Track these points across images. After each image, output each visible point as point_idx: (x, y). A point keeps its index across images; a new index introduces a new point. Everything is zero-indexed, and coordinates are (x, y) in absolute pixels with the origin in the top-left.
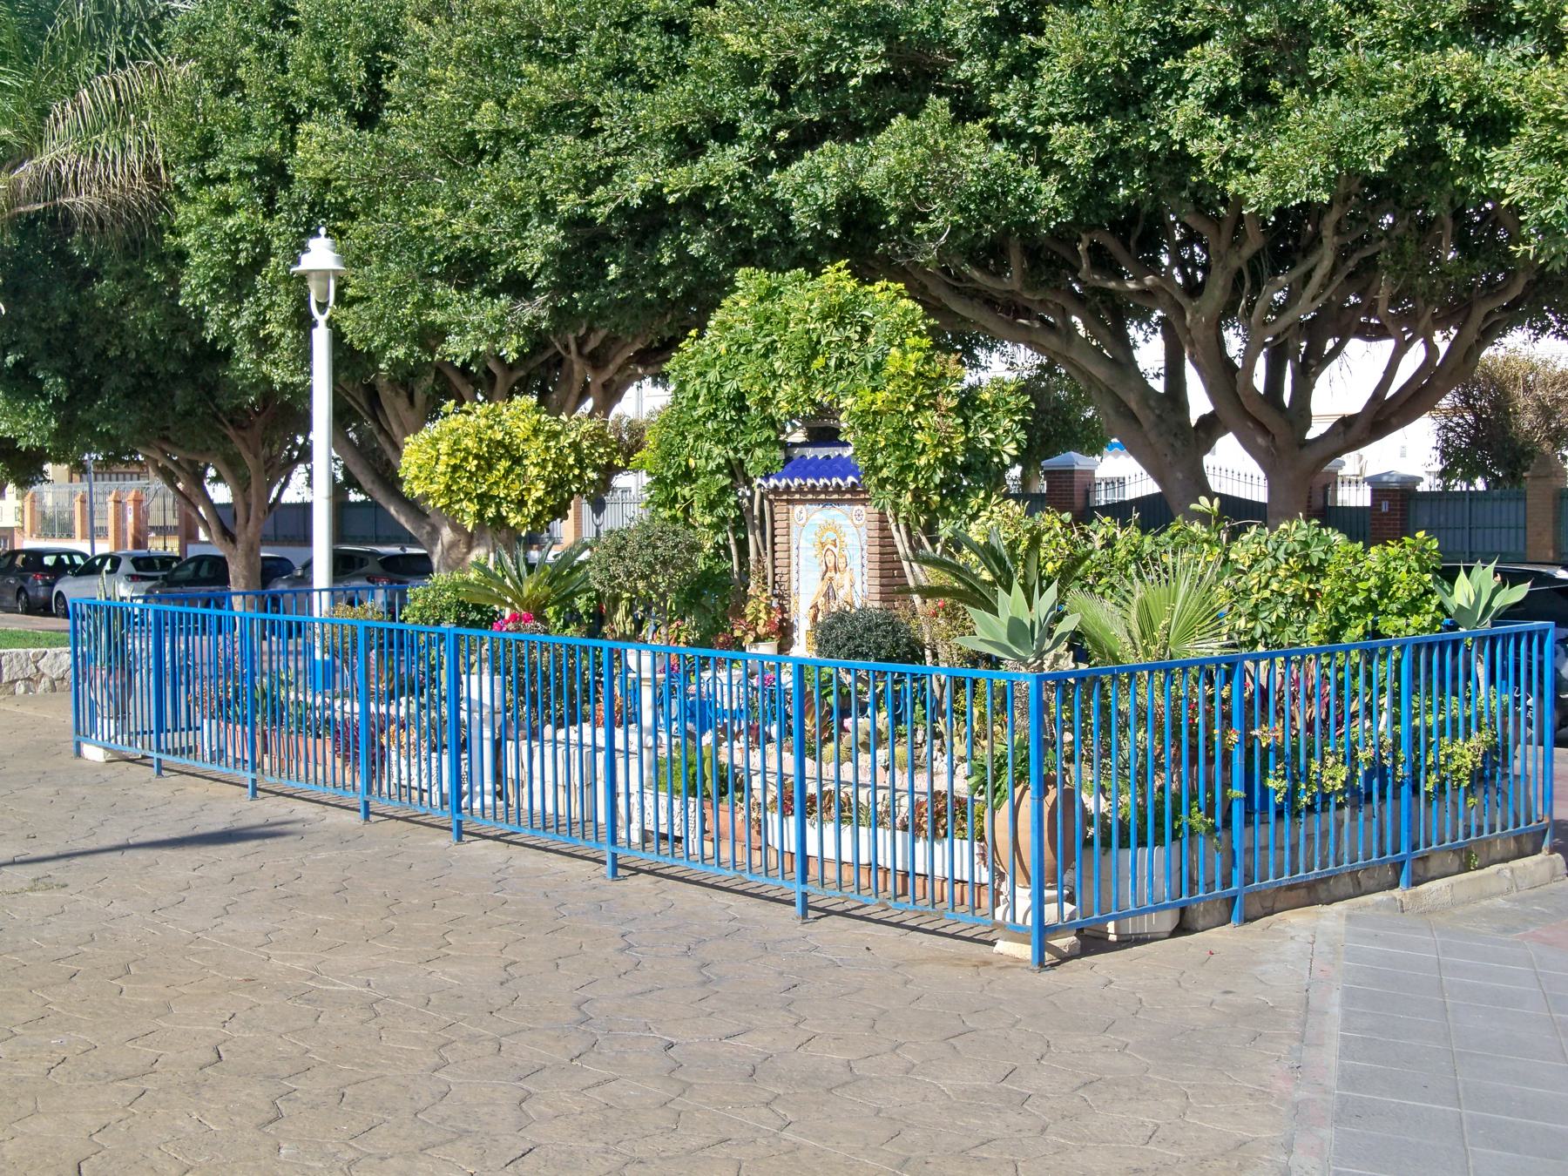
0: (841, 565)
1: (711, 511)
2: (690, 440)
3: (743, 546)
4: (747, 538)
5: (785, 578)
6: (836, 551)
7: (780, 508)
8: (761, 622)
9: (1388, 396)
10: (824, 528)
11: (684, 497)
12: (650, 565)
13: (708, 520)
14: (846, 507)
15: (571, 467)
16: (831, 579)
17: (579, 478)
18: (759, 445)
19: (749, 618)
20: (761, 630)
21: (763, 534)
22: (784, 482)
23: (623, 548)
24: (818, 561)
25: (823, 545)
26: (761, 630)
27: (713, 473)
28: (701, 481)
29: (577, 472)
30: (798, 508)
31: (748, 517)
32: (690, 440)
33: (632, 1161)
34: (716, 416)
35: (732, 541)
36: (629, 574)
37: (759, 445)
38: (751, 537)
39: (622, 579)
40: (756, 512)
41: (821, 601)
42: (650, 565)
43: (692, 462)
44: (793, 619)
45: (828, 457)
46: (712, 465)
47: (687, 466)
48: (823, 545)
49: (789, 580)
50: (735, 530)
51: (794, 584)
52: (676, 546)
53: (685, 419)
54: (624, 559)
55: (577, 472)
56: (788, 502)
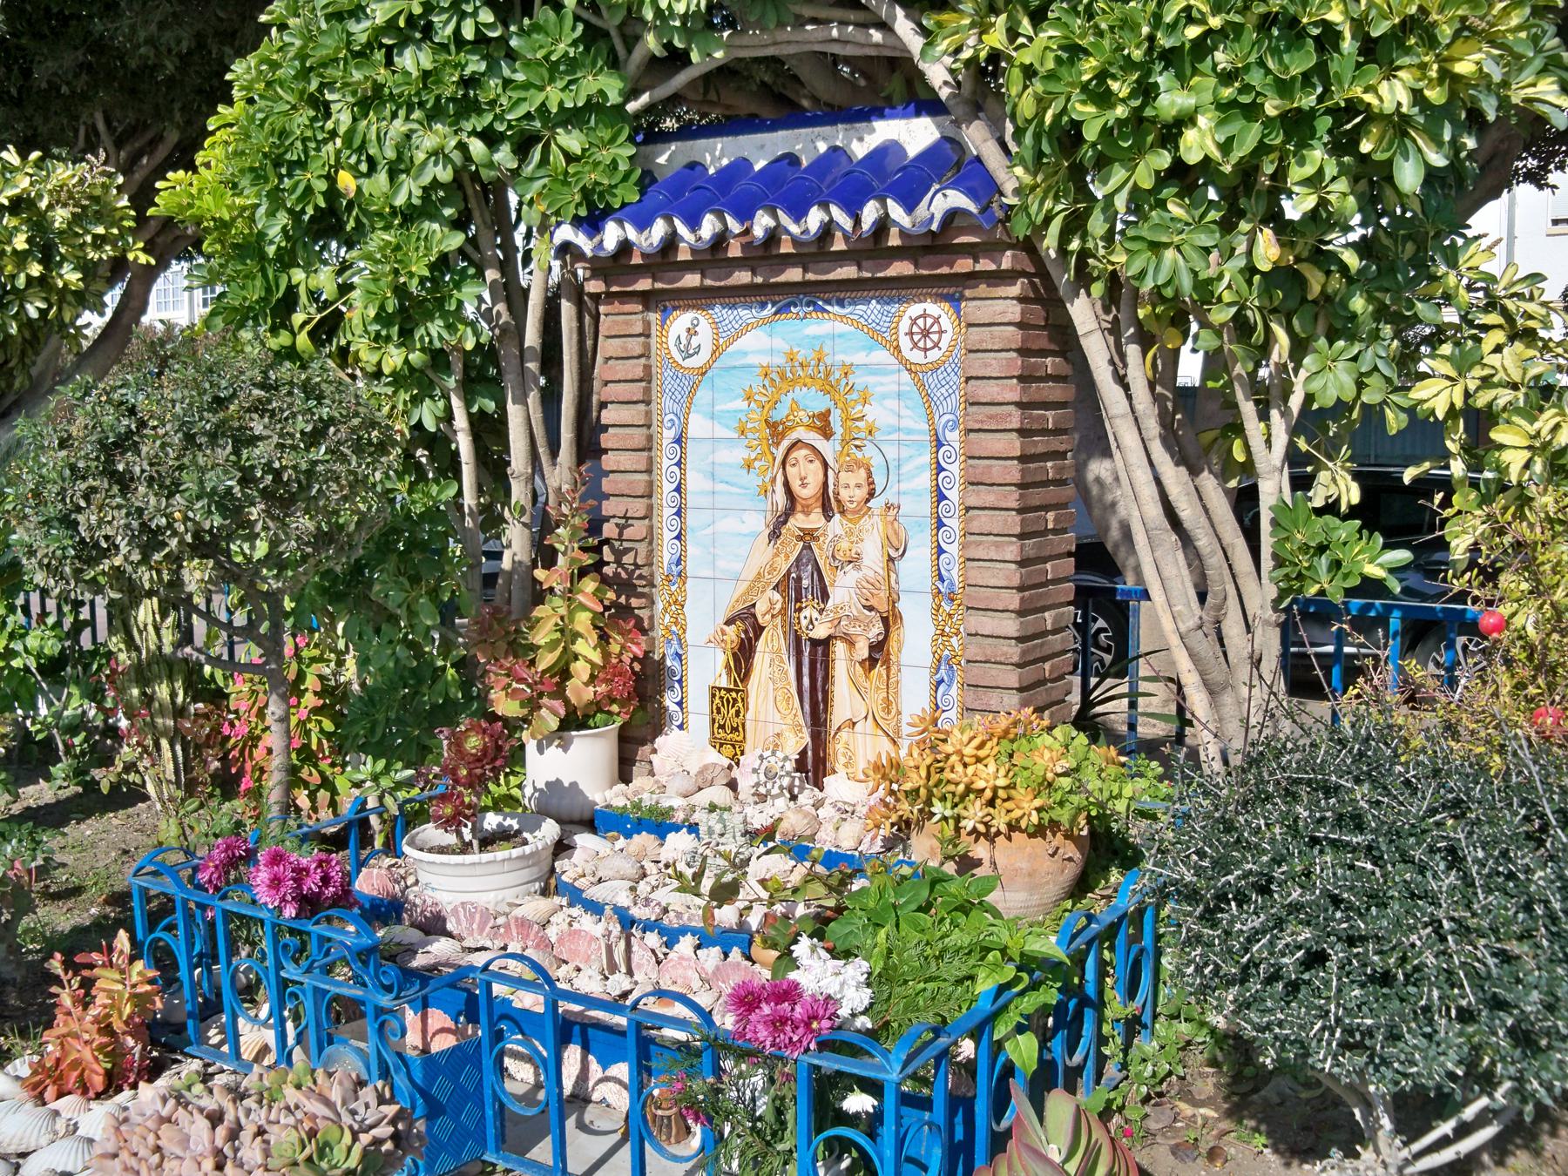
0: (850, 488)
1: (406, 335)
2: (342, 118)
3: (489, 430)
4: (502, 407)
5: (636, 530)
6: (828, 449)
7: (611, 319)
8: (581, 670)
9: (956, 241)
10: (781, 378)
11: (314, 295)
12: (225, 503)
13: (394, 358)
14: (872, 310)
15: (21, 258)
16: (808, 536)
17: (43, 282)
18: (572, 118)
19: (546, 660)
20: (580, 690)
21: (551, 398)
22: (659, 229)
23: (126, 442)
24: (753, 480)
25: (776, 430)
26: (580, 690)
27: (409, 216)
28: (380, 238)
29: (36, 270)
30: (681, 321)
31: (507, 353)
32: (342, 118)
33: (192, 674)
34: (428, 30)
35: (461, 421)
36: (149, 540)
37: (572, 118)
38: (514, 412)
39: (125, 554)
40: (532, 337)
41: (767, 603)
42: (225, 503)
43: (346, 181)
44: (664, 650)
45: (742, 165)
46: (409, 190)
47: (332, 193)
48: (776, 430)
49: (650, 538)
50: (469, 389)
51: (667, 552)
52: (314, 438)
53: (329, 45)
54: (124, 482)
55: (36, 270)
56: (648, 300)
